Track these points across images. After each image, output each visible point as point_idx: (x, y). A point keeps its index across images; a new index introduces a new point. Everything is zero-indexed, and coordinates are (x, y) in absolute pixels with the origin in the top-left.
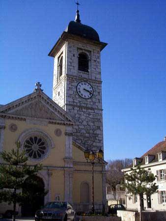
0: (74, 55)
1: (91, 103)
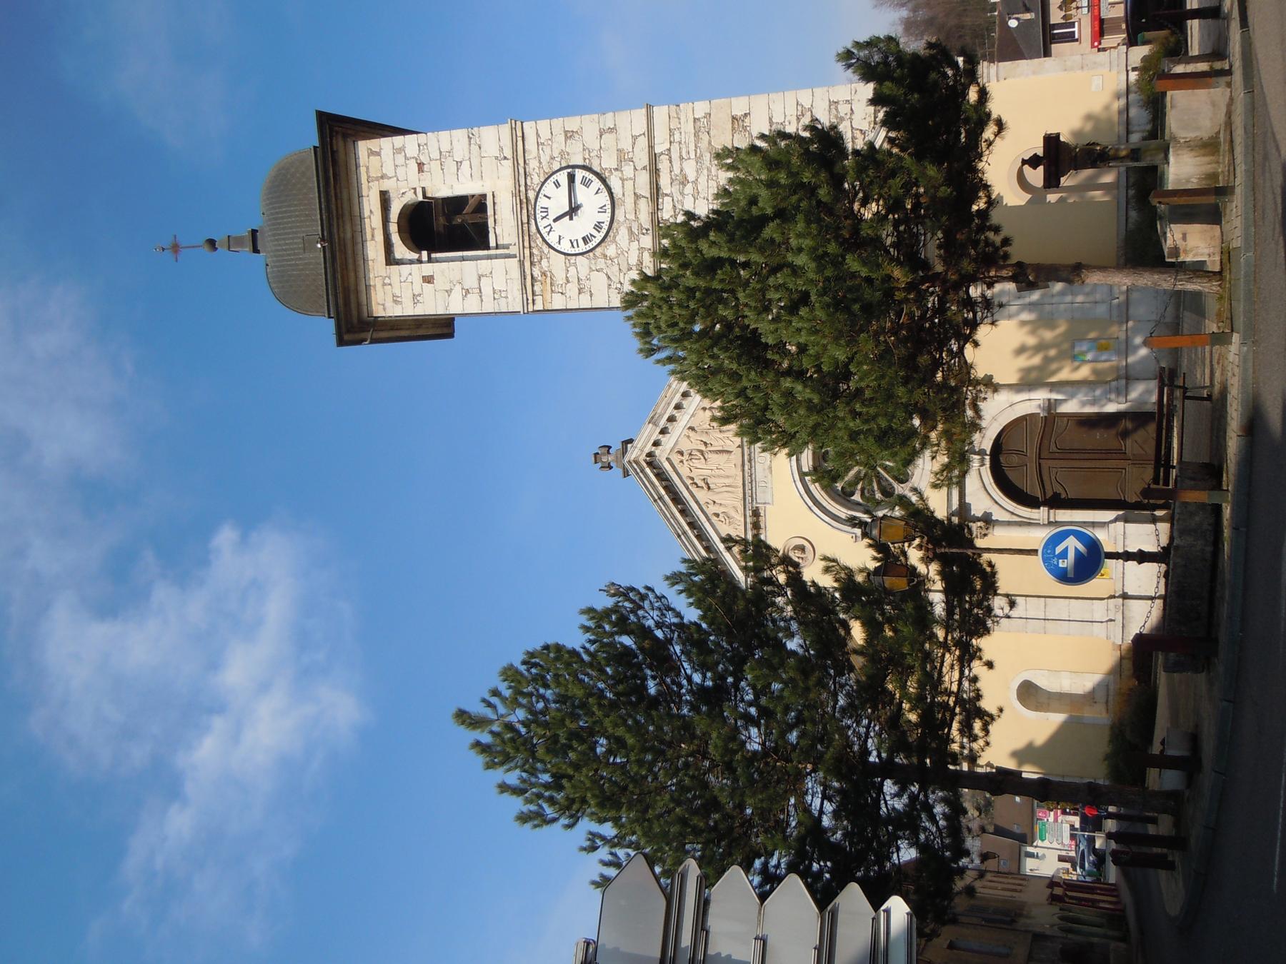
0: (428, 280)
1: (628, 170)
